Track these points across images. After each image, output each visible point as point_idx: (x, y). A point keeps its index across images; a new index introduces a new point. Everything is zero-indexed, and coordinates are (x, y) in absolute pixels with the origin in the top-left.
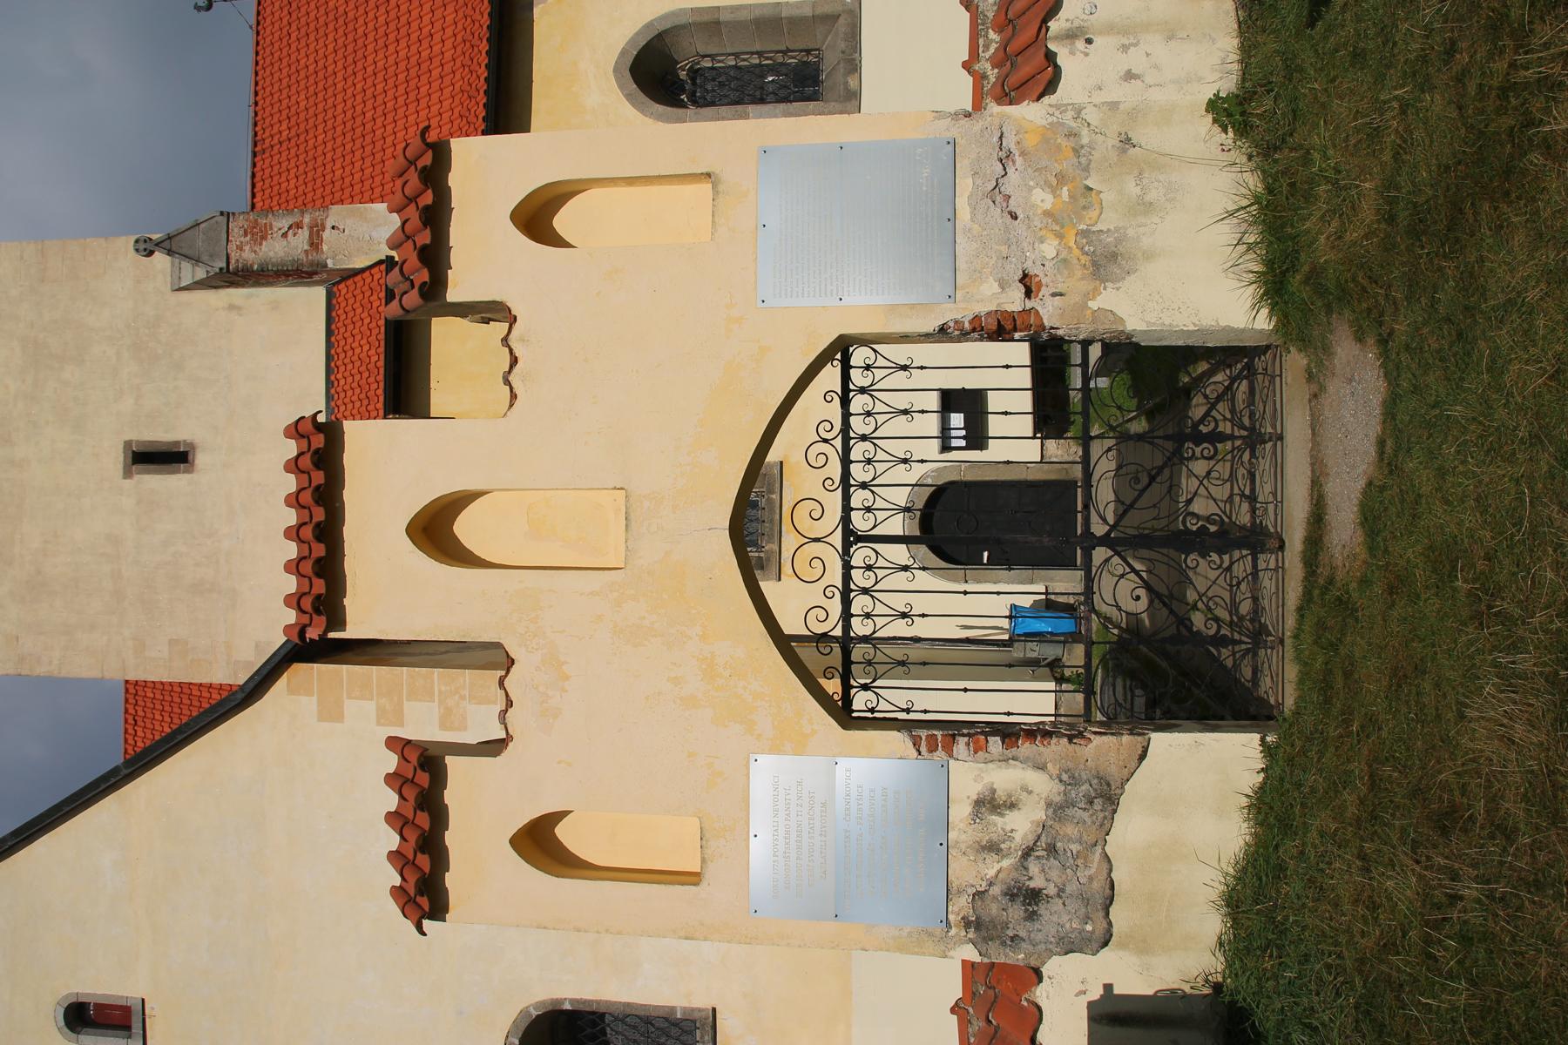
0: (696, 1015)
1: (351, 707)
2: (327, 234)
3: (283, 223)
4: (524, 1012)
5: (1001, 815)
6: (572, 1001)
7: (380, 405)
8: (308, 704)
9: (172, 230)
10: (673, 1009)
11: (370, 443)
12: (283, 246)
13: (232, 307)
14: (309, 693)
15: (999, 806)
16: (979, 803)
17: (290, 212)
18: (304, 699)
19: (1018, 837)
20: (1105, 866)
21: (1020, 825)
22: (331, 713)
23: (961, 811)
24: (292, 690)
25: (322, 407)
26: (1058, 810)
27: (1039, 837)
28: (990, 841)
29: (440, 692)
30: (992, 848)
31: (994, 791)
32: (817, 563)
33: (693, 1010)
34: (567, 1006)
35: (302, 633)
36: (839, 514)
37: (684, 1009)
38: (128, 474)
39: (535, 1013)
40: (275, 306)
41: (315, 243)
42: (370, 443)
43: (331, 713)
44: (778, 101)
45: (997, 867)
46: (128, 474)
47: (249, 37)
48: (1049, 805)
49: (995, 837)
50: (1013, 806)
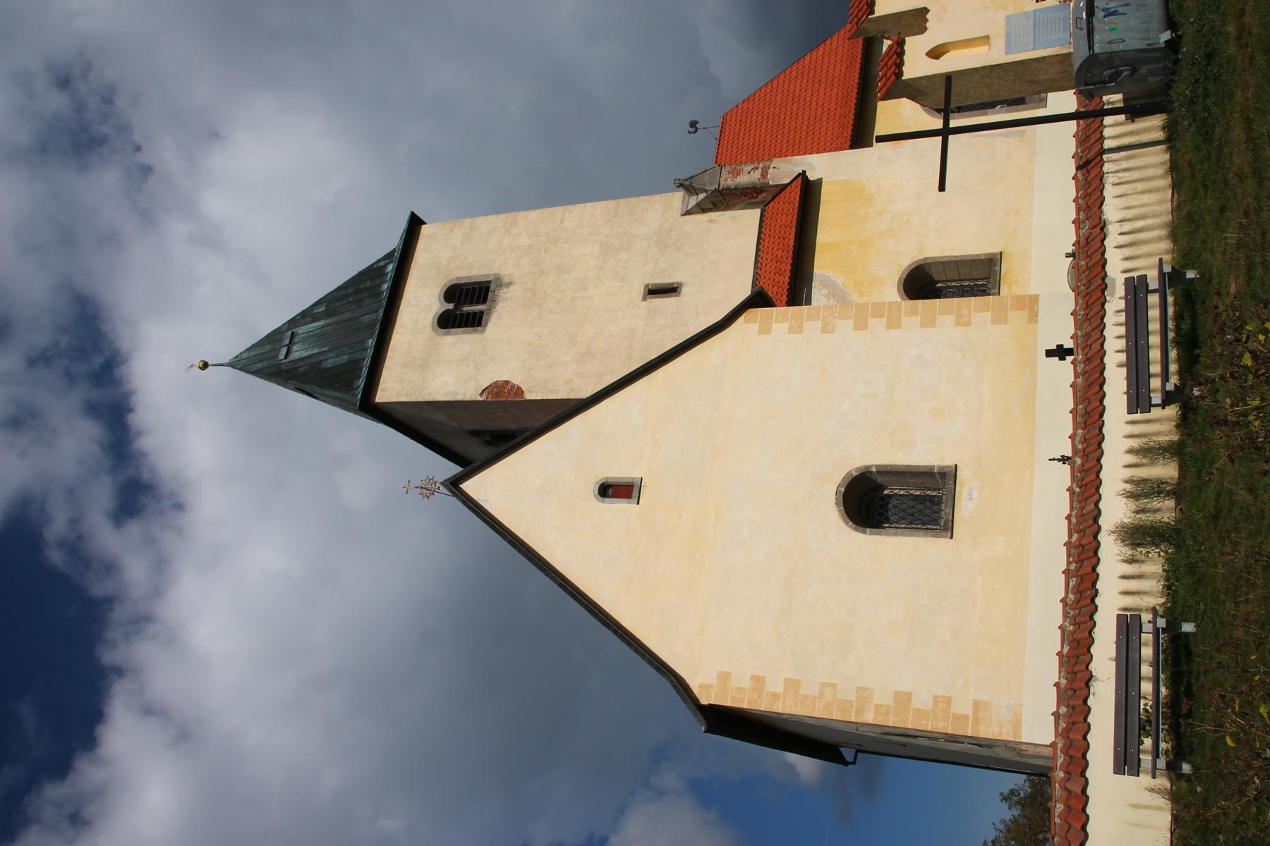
2: (770, 171)
3: (750, 168)
4: (849, 474)
6: (877, 466)
8: (754, 327)
9: (692, 174)
10: (933, 467)
12: (748, 176)
13: (711, 221)
14: (755, 322)
17: (753, 162)
22: (765, 330)
24: (746, 322)
36: (1067, 238)
37: (939, 467)
38: (644, 299)
39: (855, 474)
40: (733, 218)
41: (764, 175)
46: (644, 299)
47: (714, 144)
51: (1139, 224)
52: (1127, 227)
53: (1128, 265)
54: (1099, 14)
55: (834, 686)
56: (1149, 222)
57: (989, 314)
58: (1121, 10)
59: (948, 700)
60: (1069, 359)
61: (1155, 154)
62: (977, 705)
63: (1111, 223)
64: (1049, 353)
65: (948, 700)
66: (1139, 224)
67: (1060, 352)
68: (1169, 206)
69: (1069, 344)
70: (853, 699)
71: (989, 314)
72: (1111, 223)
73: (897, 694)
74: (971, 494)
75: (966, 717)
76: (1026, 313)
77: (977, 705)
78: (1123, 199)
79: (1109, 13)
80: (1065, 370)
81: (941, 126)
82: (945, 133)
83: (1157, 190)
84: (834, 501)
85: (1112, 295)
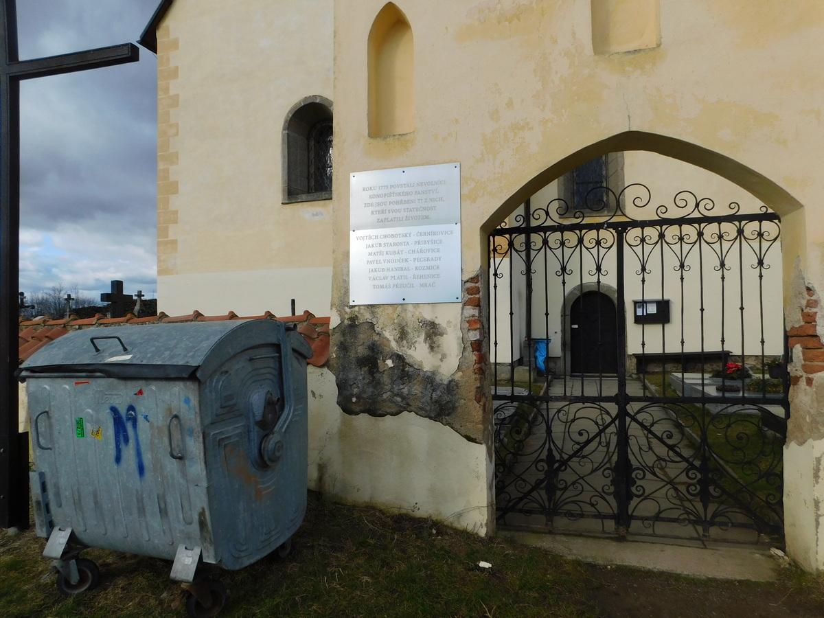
5: (425, 340)
16: (433, 325)
19: (411, 352)
20: (394, 410)
21: (419, 354)
26: (430, 380)
27: (412, 366)
30: (403, 335)
31: (441, 335)
45: (391, 338)
48: (433, 373)
49: (411, 335)
50: (432, 348)
54: (122, 395)
55: (177, 134)
59: (175, 222)
62: (174, 242)
74: (317, 215)
77: (174, 242)
79: (123, 423)
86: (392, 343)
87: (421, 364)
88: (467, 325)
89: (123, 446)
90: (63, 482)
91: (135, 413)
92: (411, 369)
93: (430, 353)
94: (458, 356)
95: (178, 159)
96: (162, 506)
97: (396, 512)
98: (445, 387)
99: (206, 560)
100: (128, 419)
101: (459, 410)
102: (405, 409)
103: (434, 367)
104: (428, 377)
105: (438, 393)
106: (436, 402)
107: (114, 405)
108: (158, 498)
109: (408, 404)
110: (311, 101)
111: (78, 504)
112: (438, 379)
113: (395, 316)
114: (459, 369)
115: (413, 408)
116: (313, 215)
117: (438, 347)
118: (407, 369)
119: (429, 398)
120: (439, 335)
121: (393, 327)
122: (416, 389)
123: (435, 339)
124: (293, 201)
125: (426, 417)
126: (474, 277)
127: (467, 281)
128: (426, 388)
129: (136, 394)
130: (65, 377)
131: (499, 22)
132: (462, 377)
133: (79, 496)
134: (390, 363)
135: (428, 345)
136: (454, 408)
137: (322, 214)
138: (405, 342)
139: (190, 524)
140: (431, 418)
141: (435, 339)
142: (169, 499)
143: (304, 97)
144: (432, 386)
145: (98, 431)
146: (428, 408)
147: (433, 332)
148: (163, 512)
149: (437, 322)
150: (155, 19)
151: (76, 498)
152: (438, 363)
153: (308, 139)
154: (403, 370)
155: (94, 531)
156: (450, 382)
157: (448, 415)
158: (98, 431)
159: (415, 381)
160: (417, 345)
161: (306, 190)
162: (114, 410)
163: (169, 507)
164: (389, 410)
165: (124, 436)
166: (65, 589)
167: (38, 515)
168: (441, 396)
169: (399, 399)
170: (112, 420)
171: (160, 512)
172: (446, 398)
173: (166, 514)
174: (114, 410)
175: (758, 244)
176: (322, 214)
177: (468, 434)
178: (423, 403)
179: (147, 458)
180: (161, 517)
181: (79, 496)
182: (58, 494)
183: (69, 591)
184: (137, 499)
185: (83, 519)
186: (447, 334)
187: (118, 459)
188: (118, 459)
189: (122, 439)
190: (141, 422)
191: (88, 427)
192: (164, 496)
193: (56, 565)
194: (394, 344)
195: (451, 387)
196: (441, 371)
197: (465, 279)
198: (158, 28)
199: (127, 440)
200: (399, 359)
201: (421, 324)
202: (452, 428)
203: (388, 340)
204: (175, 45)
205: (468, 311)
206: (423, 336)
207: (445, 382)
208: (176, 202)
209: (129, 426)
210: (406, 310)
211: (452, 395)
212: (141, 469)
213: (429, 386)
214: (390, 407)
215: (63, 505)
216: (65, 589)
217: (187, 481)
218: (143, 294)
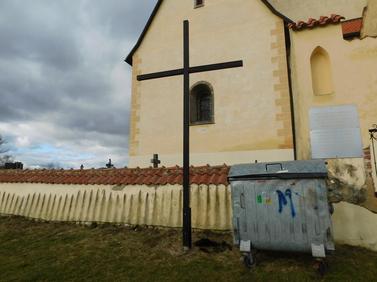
0: (213, 120)
1: (274, 37)
4: (210, 84)
5: (348, 172)
6: (213, 94)
7: (345, 33)
8: (274, 27)
10: (214, 115)
11: (337, 31)
14: (277, 27)
15: (351, 172)
16: (351, 166)
18: (275, 26)
19: (342, 177)
20: (336, 201)
21: (346, 177)
22: (272, 33)
23: (348, 162)
24: (277, 23)
25: (346, 19)
26: (352, 188)
27: (343, 183)
28: (339, 170)
29: (280, 56)
30: (337, 170)
31: (355, 170)
32: (374, 126)
33: (214, 119)
34: (212, 93)
35: (32, 171)
37: (214, 117)
39: (210, 86)
42: (337, 31)
43: (272, 33)
44: (289, 148)
45: (332, 172)
48: (353, 185)
49: (341, 171)
50: (351, 176)
51: (151, 206)
52: (151, 198)
53: (128, 198)
54: (283, 186)
55: (140, 97)
56: (151, 211)
57: (283, 128)
58: (287, 209)
59: (138, 133)
60: (152, 165)
61: (179, 220)
62: (138, 142)
63: (156, 189)
64: (156, 156)
65: (138, 133)
66: (151, 206)
67: (156, 161)
68: (157, 223)
69: (160, 166)
70: (137, 104)
71: (283, 128)
72: (156, 189)
73: (139, 117)
74: (204, 130)
75: (134, 139)
76: (284, 144)
77: (138, 142)
78: (21, 200)
79: (282, 198)
80: (146, 163)
81: (181, 66)
82: (186, 71)
83: (170, 218)
84: (199, 81)
85: (114, 189)
86: (332, 174)
87: (347, 182)
88: (367, 166)
89: (283, 205)
90: (248, 222)
91: (290, 192)
92: (342, 184)
93: (351, 177)
94: (364, 178)
95: (140, 107)
96: (304, 228)
97: (342, 243)
98: (359, 191)
99: (329, 248)
100: (287, 195)
101: (367, 200)
102: (341, 200)
103: (353, 183)
104: (351, 187)
105: (356, 193)
106: (355, 197)
107: (279, 190)
108: (302, 225)
109: (342, 198)
110: (199, 83)
111: (256, 230)
112: (355, 188)
113: (333, 163)
114: (365, 184)
115: (345, 200)
116: (202, 130)
117: (354, 175)
118: (340, 184)
119: (352, 196)
120: (354, 170)
121: (332, 167)
122: (346, 192)
123: (353, 172)
124: (193, 125)
125: (352, 203)
126: (368, 148)
127: (365, 149)
128: (350, 192)
129: (292, 185)
130: (252, 180)
131: (368, 53)
132: (367, 187)
133: (257, 226)
134: (332, 182)
135: (349, 174)
136: (365, 200)
137: (206, 130)
138: (338, 173)
139: (319, 235)
140: (354, 204)
141: (353, 172)
142: (309, 226)
143: (197, 81)
144: (353, 191)
145: (269, 200)
146: (352, 200)
147: (352, 169)
148: (304, 231)
149: (353, 165)
150: (134, 50)
151: (256, 227)
152: (355, 181)
153: (197, 99)
154: (339, 185)
155: (263, 240)
156: (362, 189)
157: (362, 202)
158: (269, 200)
159: (345, 189)
160: (344, 174)
161: (196, 120)
162: (279, 192)
163: (308, 228)
164: (334, 201)
165: (284, 201)
166: (248, 265)
167: (235, 235)
168: (357, 195)
169: (338, 196)
170: (278, 196)
171: (303, 231)
172: (360, 196)
173: (306, 231)
174: (279, 192)
175: (293, 150)
176: (206, 130)
177: (373, 210)
178: (349, 198)
179: (297, 210)
180: (303, 233)
181: (257, 226)
182: (245, 226)
183: (251, 266)
184: (290, 226)
185: (258, 236)
186: (358, 170)
187: (280, 210)
188: (280, 210)
189: (282, 202)
190: (293, 195)
191: (264, 199)
192: (306, 224)
193: (246, 255)
194: (333, 174)
195: (362, 191)
196: (356, 185)
197: (364, 148)
198: (133, 55)
199: (285, 203)
200: (337, 180)
201: (345, 166)
202: (365, 207)
203: (331, 172)
204: (140, 61)
205: (366, 161)
206: (347, 171)
207: (359, 189)
208: (138, 125)
209: (287, 198)
210: (338, 161)
211: (363, 194)
212: (293, 214)
213: (351, 191)
214: (334, 200)
215: (247, 231)
216: (248, 265)
217: (319, 217)
218: (83, 166)
